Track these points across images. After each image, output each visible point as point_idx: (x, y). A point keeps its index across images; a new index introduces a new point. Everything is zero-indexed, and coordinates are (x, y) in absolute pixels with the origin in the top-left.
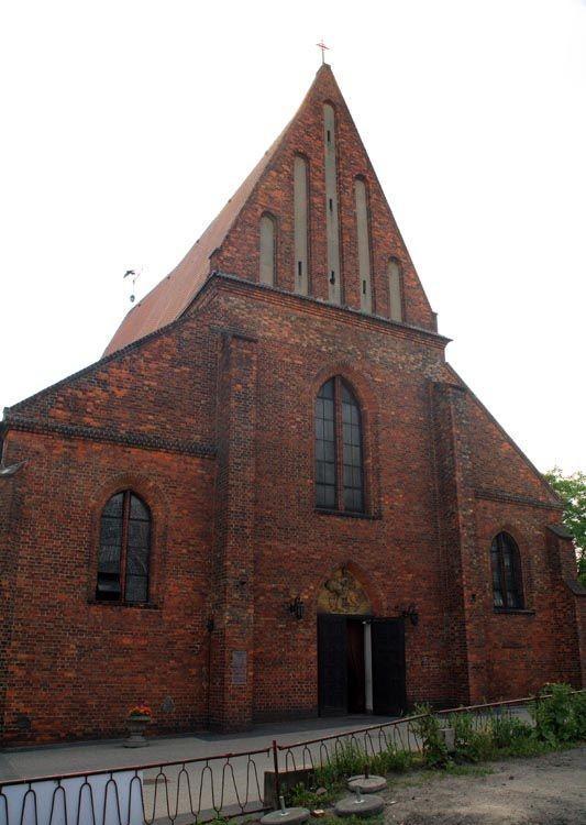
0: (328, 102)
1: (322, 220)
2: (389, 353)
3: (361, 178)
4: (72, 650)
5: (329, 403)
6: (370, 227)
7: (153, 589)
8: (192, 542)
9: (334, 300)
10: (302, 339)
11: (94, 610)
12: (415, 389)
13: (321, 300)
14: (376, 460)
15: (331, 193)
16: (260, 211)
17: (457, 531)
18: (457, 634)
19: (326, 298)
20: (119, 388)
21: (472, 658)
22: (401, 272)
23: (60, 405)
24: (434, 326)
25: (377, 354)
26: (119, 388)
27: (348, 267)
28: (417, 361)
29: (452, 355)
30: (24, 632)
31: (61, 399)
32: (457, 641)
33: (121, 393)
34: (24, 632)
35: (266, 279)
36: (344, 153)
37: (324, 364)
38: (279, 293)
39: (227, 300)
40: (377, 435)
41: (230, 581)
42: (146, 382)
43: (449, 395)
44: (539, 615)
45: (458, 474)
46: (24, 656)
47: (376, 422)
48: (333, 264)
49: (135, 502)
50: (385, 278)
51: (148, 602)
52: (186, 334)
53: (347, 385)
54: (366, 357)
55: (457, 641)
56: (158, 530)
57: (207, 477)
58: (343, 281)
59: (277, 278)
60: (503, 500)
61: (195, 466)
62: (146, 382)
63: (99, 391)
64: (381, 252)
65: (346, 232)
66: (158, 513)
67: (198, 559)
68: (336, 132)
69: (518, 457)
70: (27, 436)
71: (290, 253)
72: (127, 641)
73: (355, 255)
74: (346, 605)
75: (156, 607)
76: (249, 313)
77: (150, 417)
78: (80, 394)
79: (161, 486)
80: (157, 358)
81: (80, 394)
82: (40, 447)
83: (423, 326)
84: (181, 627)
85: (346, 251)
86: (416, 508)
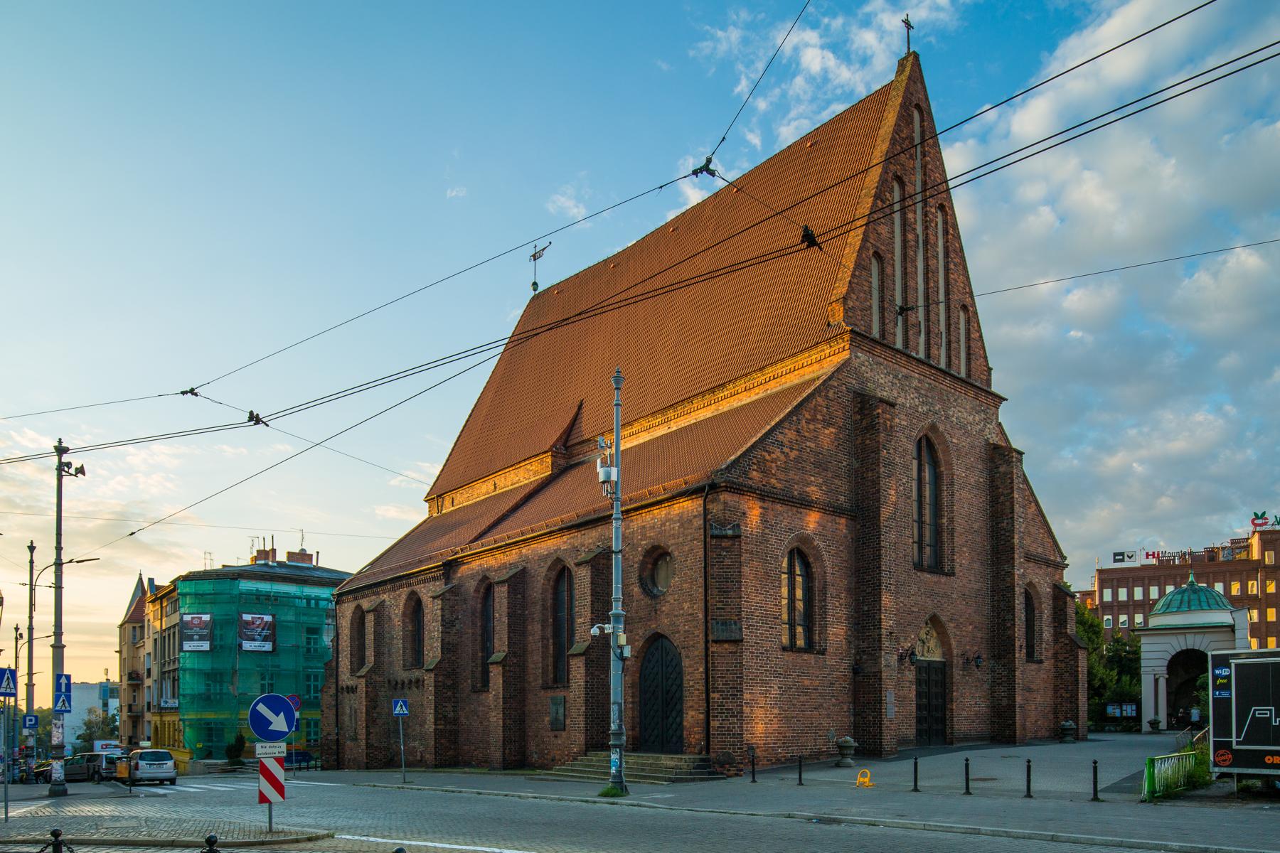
2: (962, 411)
16: (871, 252)
22: (968, 322)
24: (989, 385)
26: (791, 449)
29: (1005, 415)
33: (793, 454)
35: (875, 333)
45: (1016, 536)
53: (930, 446)
54: (947, 418)
58: (928, 333)
63: (778, 453)
69: (1033, 508)
72: (807, 683)
78: (767, 457)
80: (814, 420)
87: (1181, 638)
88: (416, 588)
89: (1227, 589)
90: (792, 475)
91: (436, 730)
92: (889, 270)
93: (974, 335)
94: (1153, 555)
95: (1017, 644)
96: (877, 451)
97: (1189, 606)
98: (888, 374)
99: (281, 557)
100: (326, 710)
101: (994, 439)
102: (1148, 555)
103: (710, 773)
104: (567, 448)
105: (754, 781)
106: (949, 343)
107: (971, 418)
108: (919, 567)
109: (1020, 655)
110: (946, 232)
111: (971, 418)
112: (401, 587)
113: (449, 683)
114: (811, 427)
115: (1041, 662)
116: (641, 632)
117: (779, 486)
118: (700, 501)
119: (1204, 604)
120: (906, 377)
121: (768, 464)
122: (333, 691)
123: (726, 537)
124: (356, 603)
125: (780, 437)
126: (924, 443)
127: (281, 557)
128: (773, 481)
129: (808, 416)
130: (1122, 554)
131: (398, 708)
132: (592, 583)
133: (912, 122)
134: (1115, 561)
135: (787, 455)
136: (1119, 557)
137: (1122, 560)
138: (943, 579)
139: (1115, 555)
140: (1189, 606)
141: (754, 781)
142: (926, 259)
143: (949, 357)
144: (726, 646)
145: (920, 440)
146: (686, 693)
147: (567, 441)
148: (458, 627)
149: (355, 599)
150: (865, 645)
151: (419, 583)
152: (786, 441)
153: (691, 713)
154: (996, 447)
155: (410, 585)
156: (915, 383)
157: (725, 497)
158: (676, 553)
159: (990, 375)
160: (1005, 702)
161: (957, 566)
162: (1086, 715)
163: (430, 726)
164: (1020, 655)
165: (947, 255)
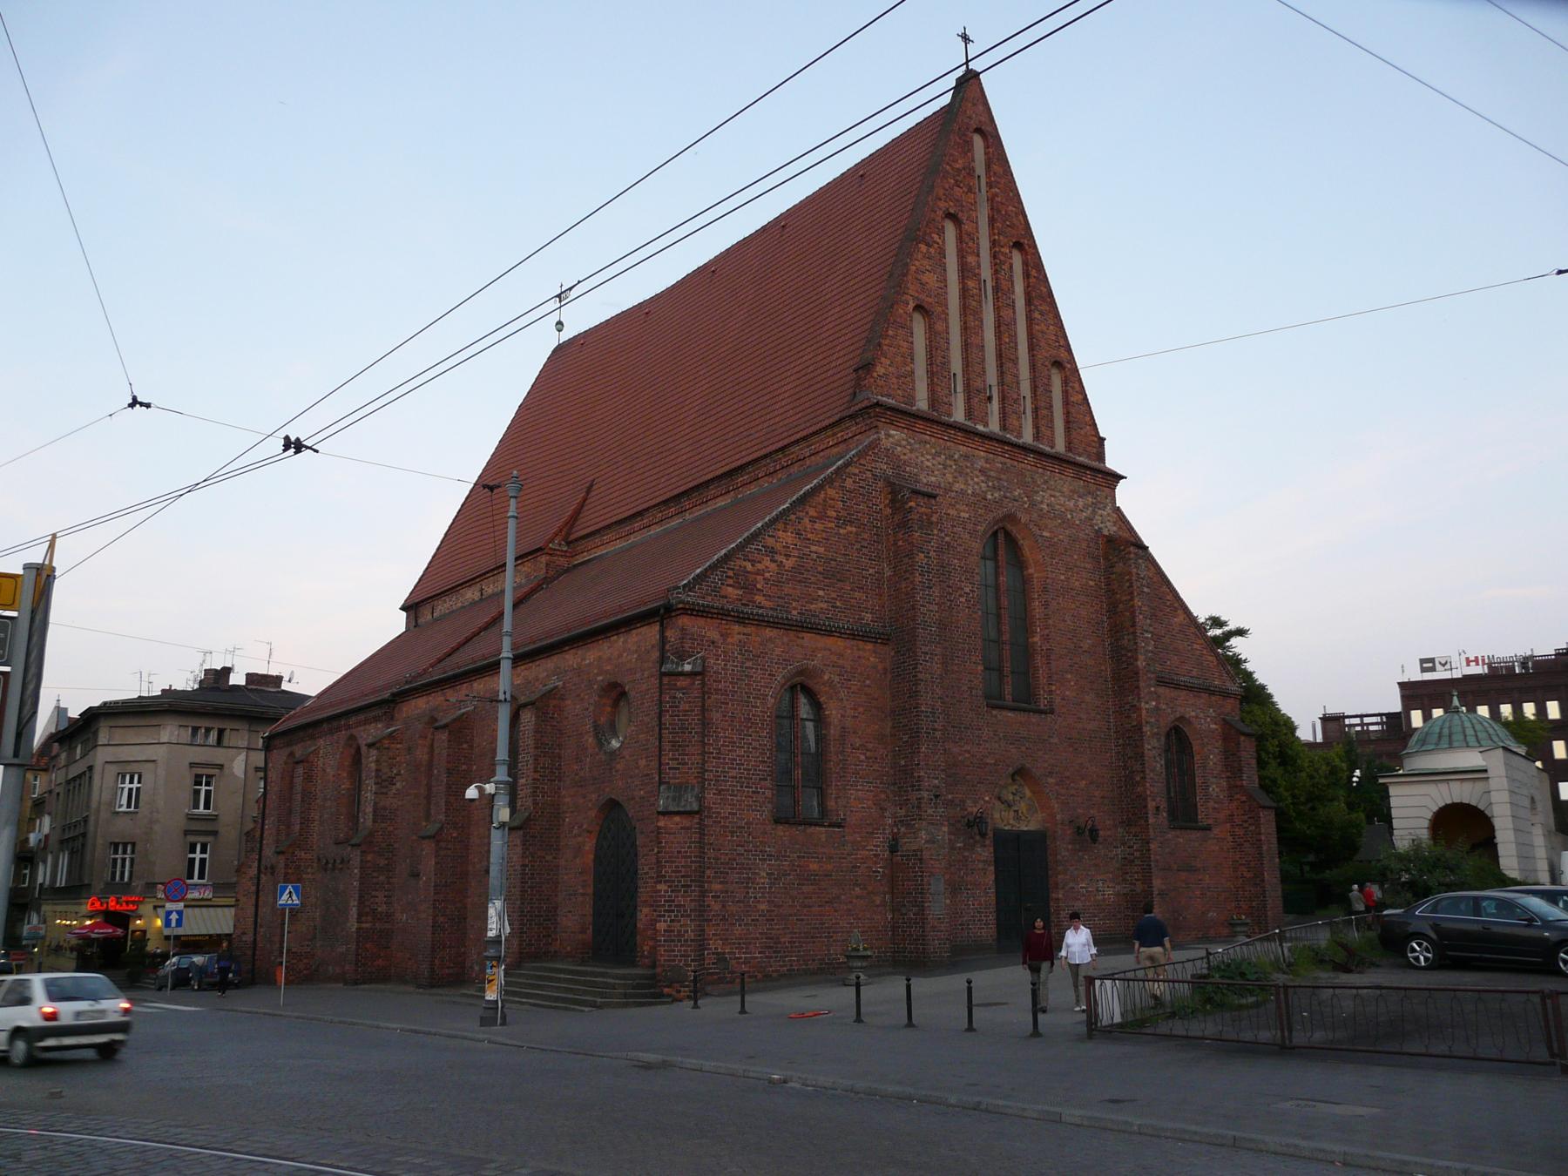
0: (978, 131)
1: (978, 314)
2: (1058, 495)
3: (1018, 245)
4: (763, 878)
5: (990, 564)
6: (1030, 321)
7: (831, 804)
8: (870, 746)
9: (994, 426)
10: (966, 484)
11: (781, 830)
12: (1084, 545)
13: (980, 428)
14: (1046, 638)
15: (986, 273)
16: (912, 305)
17: (1139, 728)
18: (1137, 854)
19: (986, 425)
20: (788, 556)
21: (1157, 883)
22: (1065, 382)
23: (730, 582)
24: (1101, 457)
25: (1044, 499)
26: (788, 556)
27: (1008, 378)
28: (1086, 506)
29: (1124, 496)
30: (717, 859)
31: (731, 573)
32: (1137, 862)
33: (789, 563)
34: (717, 859)
35: (922, 404)
36: (999, 211)
37: (991, 515)
38: (934, 422)
39: (888, 435)
40: (1046, 605)
41: (925, 794)
42: (814, 548)
43: (1123, 551)
44: (1216, 831)
45: (1141, 657)
46: (719, 887)
47: (1045, 590)
48: (992, 377)
49: (802, 700)
50: (1048, 385)
51: (824, 818)
52: (849, 483)
53: (1011, 541)
54: (1033, 505)
55: (1137, 862)
56: (833, 732)
57: (880, 667)
58: (1003, 399)
59: (933, 402)
60: (1177, 686)
61: (870, 656)
62: (814, 548)
63: (767, 562)
64: (1044, 354)
65: (1003, 327)
66: (833, 712)
67: (876, 767)
68: (988, 177)
69: (1181, 618)
70: (701, 622)
71: (946, 364)
72: (814, 867)
73: (1015, 362)
74: (1018, 818)
75: (839, 826)
76: (911, 451)
77: (821, 593)
78: (749, 566)
79: (837, 679)
80: (822, 516)
81: (749, 566)
82: (714, 635)
83: (1089, 457)
84: (864, 848)
85: (1005, 358)
86: (1088, 698)
87: (1443, 787)
88: (354, 732)
89: (1495, 713)
90: (787, 589)
91: (359, 929)
92: (939, 326)
93: (1075, 398)
94: (1476, 660)
95: (1151, 805)
96: (910, 555)
97: (1450, 742)
98: (938, 454)
99: (237, 679)
100: (243, 900)
101: (1110, 528)
102: (1468, 662)
103: (653, 996)
104: (568, 543)
105: (696, 1006)
106: (1036, 410)
107: (1071, 504)
108: (994, 701)
109: (1157, 820)
110: (1027, 275)
111: (1071, 504)
112: (339, 729)
113: (383, 862)
114: (817, 526)
115: (1208, 828)
116: (594, 797)
117: (767, 604)
118: (657, 627)
119: (1472, 740)
120: (966, 457)
121: (751, 577)
122: (253, 871)
123: (682, 674)
124: (288, 750)
125: (770, 542)
126: (1001, 536)
127: (237, 679)
128: (759, 598)
129: (812, 512)
130: (1432, 660)
131: (285, 896)
132: (536, 732)
133: (971, 149)
134: (1424, 670)
135: (781, 565)
136: (1427, 664)
137: (1433, 669)
138: (1034, 718)
139: (1422, 661)
140: (1450, 742)
141: (696, 1006)
142: (997, 309)
143: (1036, 427)
144: (677, 819)
145: (995, 534)
146: (640, 883)
147: (568, 534)
148: (398, 785)
149: (288, 745)
150: (903, 812)
151: (359, 724)
152: (778, 547)
153: (646, 910)
154: (1110, 540)
155: (349, 727)
156: (980, 464)
157: (684, 621)
158: (632, 694)
159: (1102, 446)
160: (1139, 887)
161: (1058, 700)
162: (1280, 902)
163: (353, 925)
164: (1157, 820)
165: (1029, 302)
